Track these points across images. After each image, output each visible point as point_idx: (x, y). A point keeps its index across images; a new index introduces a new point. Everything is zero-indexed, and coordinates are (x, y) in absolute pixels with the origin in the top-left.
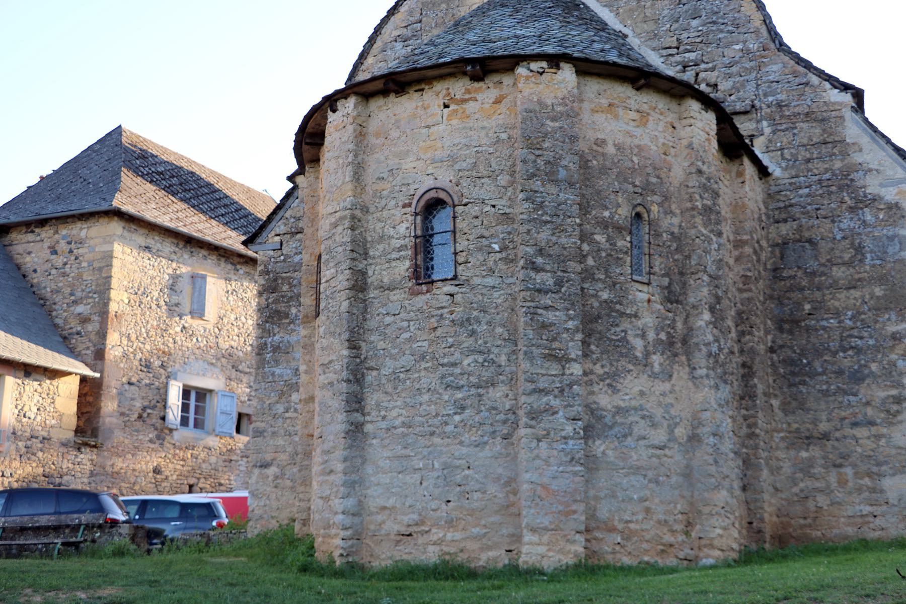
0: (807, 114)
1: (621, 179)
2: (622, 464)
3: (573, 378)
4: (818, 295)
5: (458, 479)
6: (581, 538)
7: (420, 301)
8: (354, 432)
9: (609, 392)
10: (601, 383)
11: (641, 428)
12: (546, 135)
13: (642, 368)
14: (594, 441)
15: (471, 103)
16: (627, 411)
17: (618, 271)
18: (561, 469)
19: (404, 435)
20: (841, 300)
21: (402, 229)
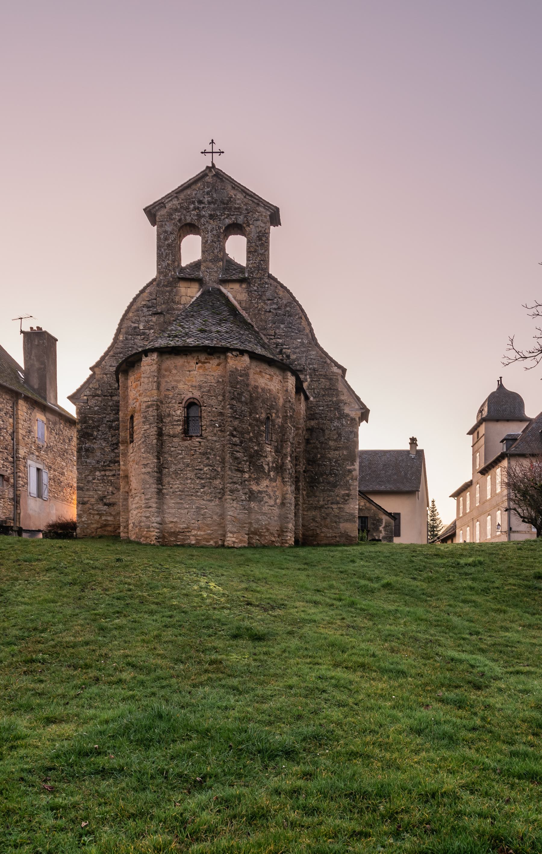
0: (325, 376)
4: (323, 451)
5: (202, 512)
6: (247, 536)
7: (186, 443)
11: (266, 499)
12: (238, 382)
15: (208, 364)
19: (180, 495)
20: (332, 454)
21: (178, 412)
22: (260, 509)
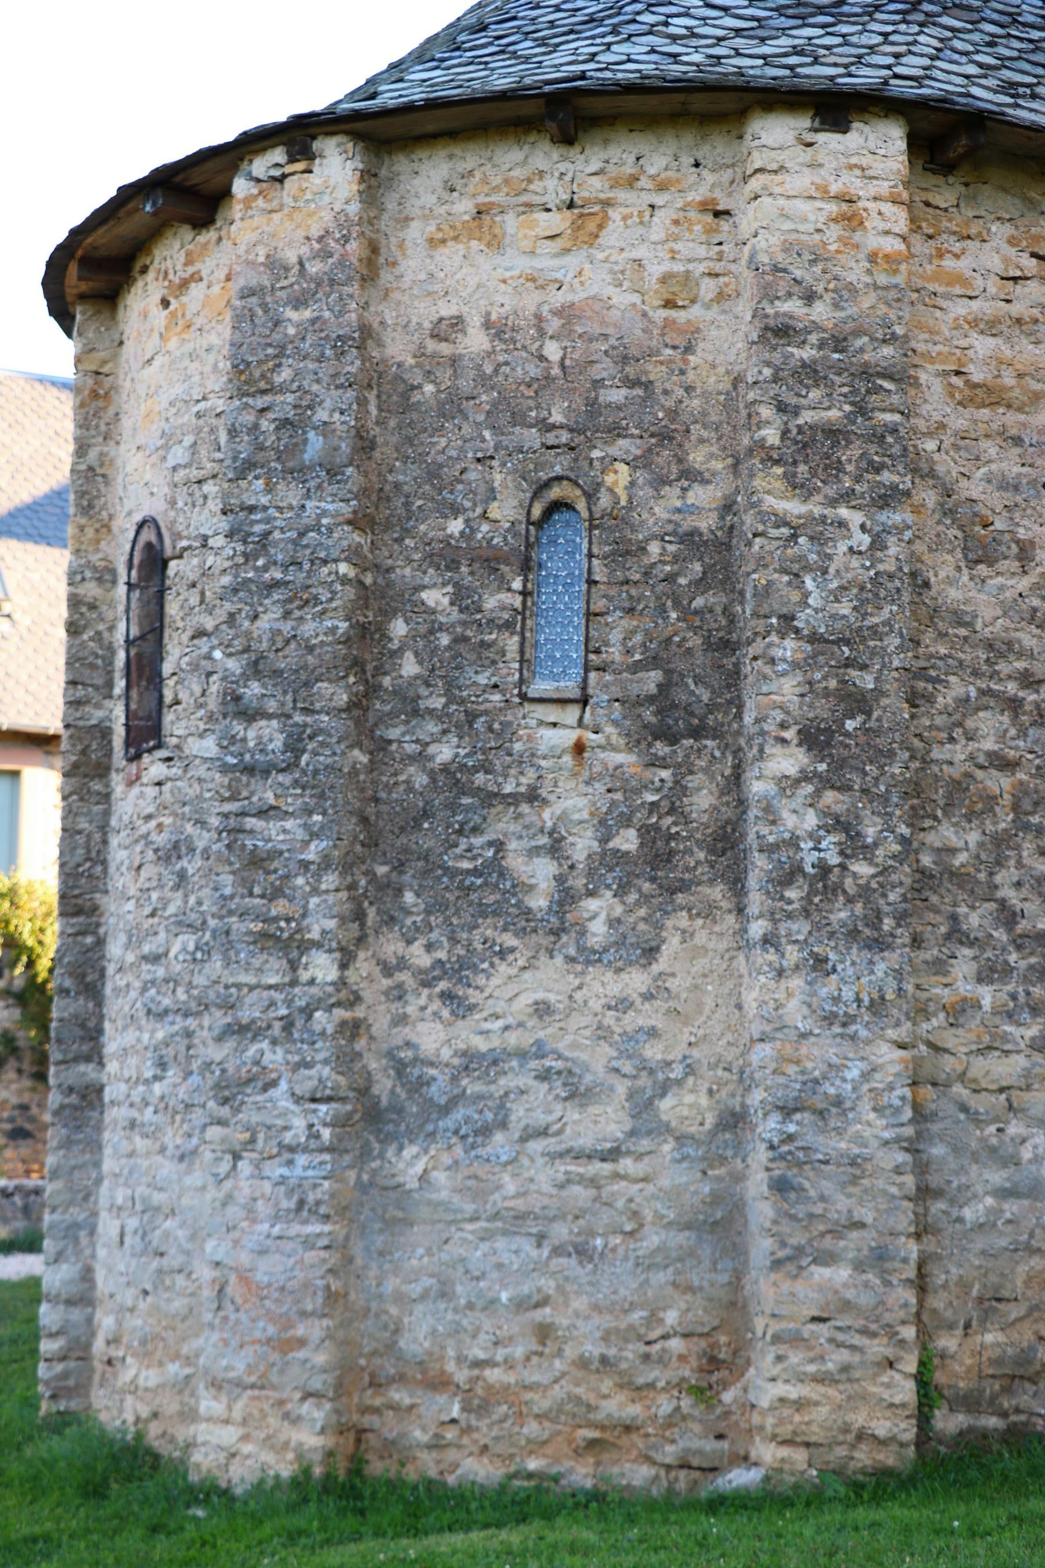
1: (504, 418)
2: (469, 1208)
3: (314, 990)
8: (75, 1108)
9: (446, 1013)
10: (426, 992)
11: (536, 1104)
13: (546, 941)
14: (401, 1148)
16: (495, 1062)
17: (482, 679)
18: (276, 1230)
22: (478, 1189)
